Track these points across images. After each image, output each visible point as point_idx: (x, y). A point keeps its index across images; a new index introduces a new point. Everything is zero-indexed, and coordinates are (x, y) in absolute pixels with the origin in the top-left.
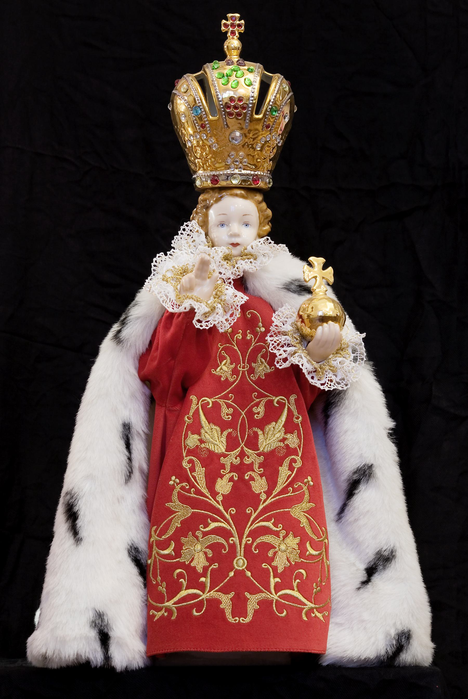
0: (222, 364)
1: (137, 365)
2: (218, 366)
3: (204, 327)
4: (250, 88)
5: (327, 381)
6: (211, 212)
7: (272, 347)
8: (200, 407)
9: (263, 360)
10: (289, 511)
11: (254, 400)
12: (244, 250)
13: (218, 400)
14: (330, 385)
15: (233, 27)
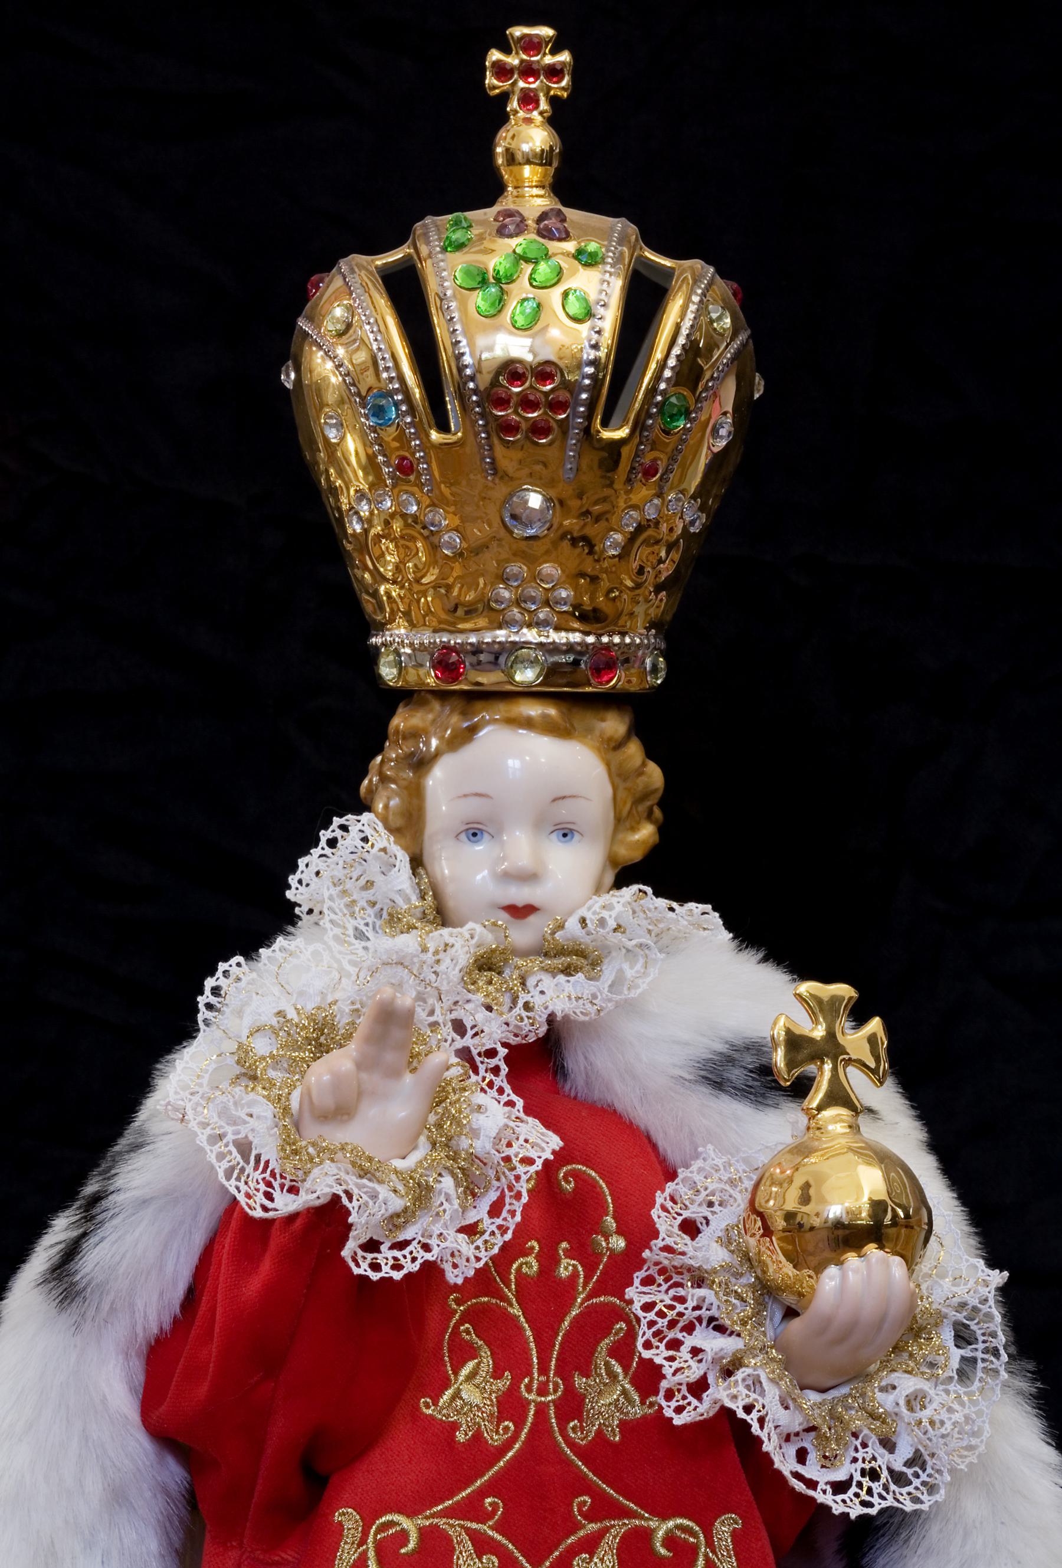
0: (461, 1378)
1: (140, 1378)
2: (446, 1385)
3: (386, 1271)
4: (584, 329)
5: (857, 1477)
6: (439, 780)
7: (649, 1333)
8: (371, 1554)
9: (618, 1369)
11: (578, 1527)
12: (553, 933)
13: (441, 1522)
14: (870, 1492)
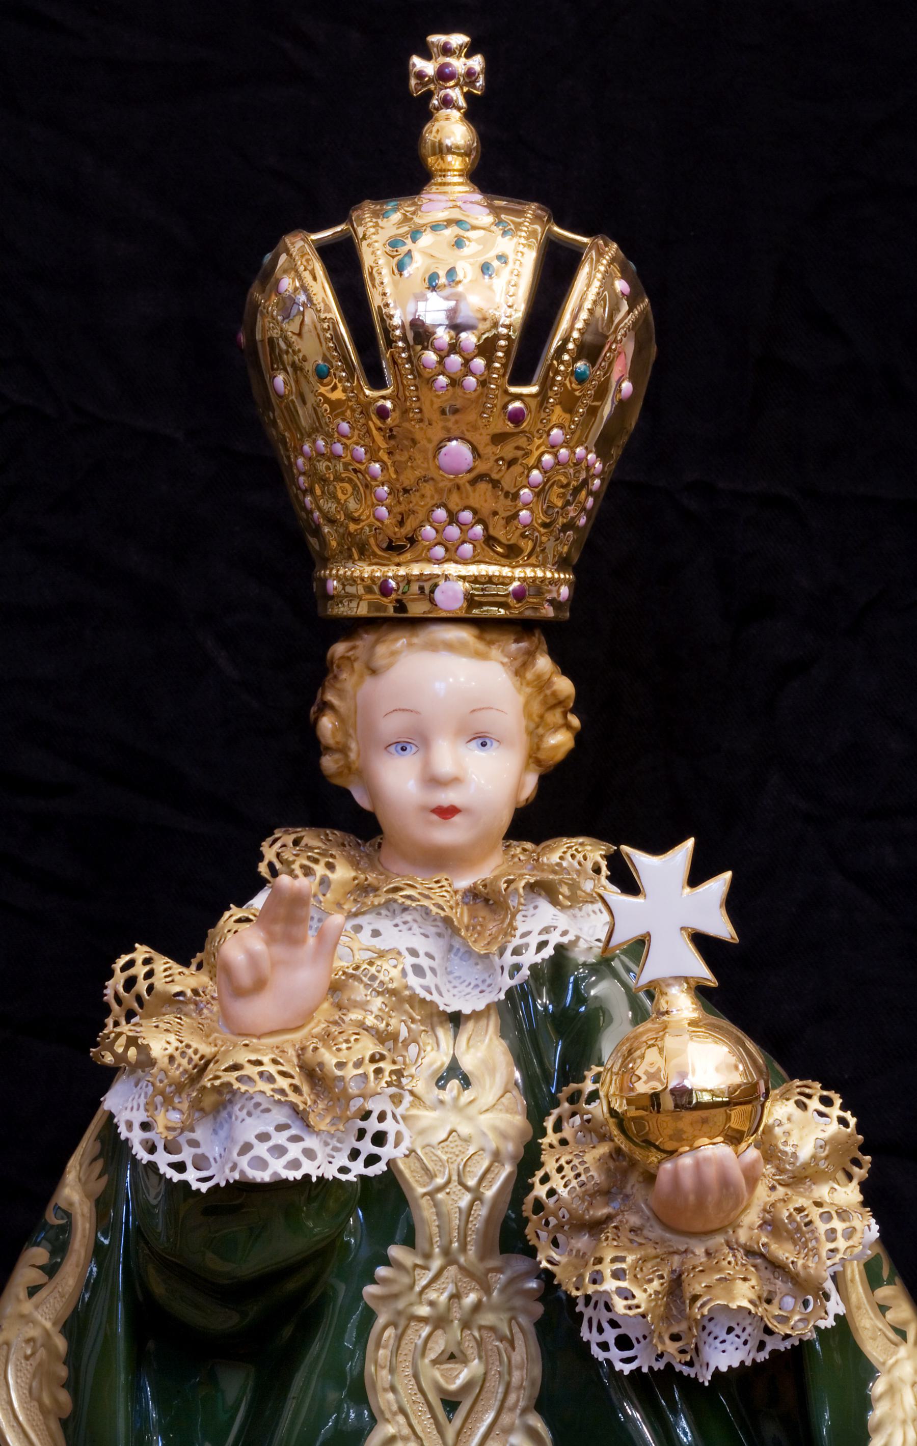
10: (766, 1125)
15: (451, 61)
